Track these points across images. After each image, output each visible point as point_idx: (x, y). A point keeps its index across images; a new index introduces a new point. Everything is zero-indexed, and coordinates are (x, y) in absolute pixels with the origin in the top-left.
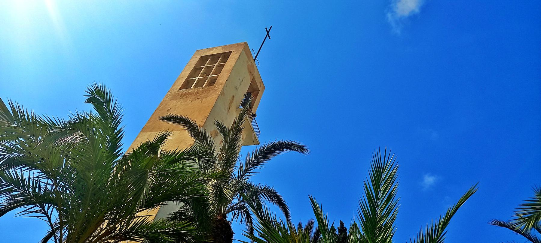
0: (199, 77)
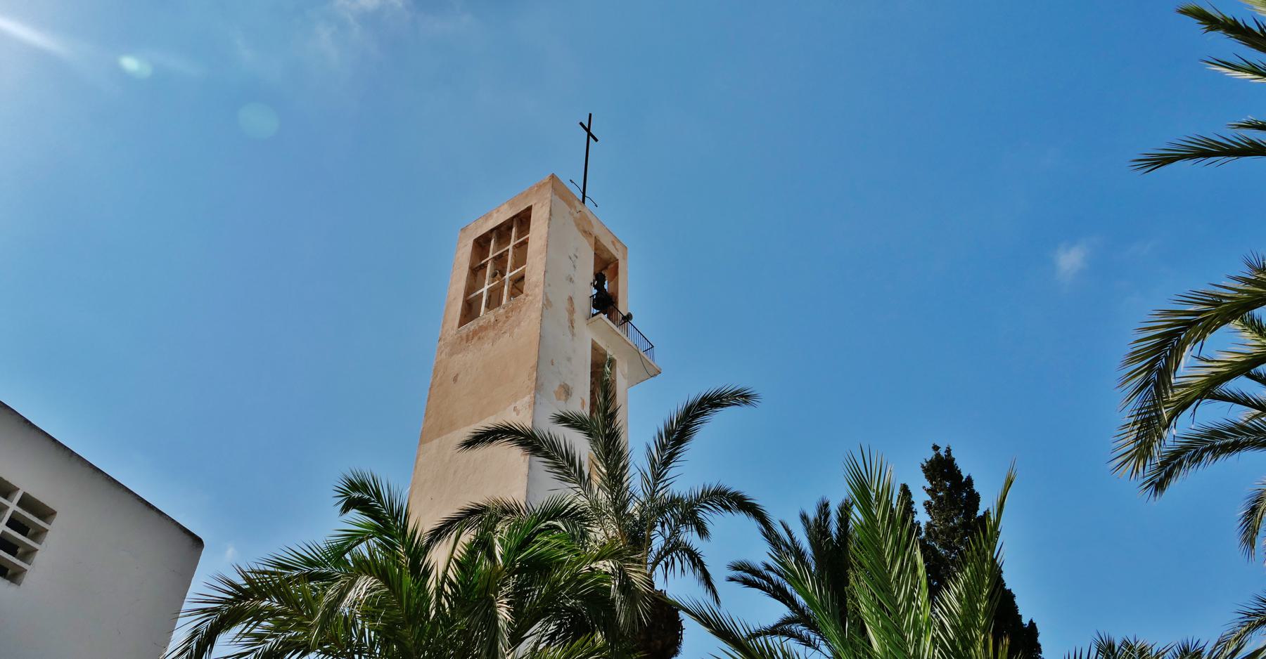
0: (487, 287)
